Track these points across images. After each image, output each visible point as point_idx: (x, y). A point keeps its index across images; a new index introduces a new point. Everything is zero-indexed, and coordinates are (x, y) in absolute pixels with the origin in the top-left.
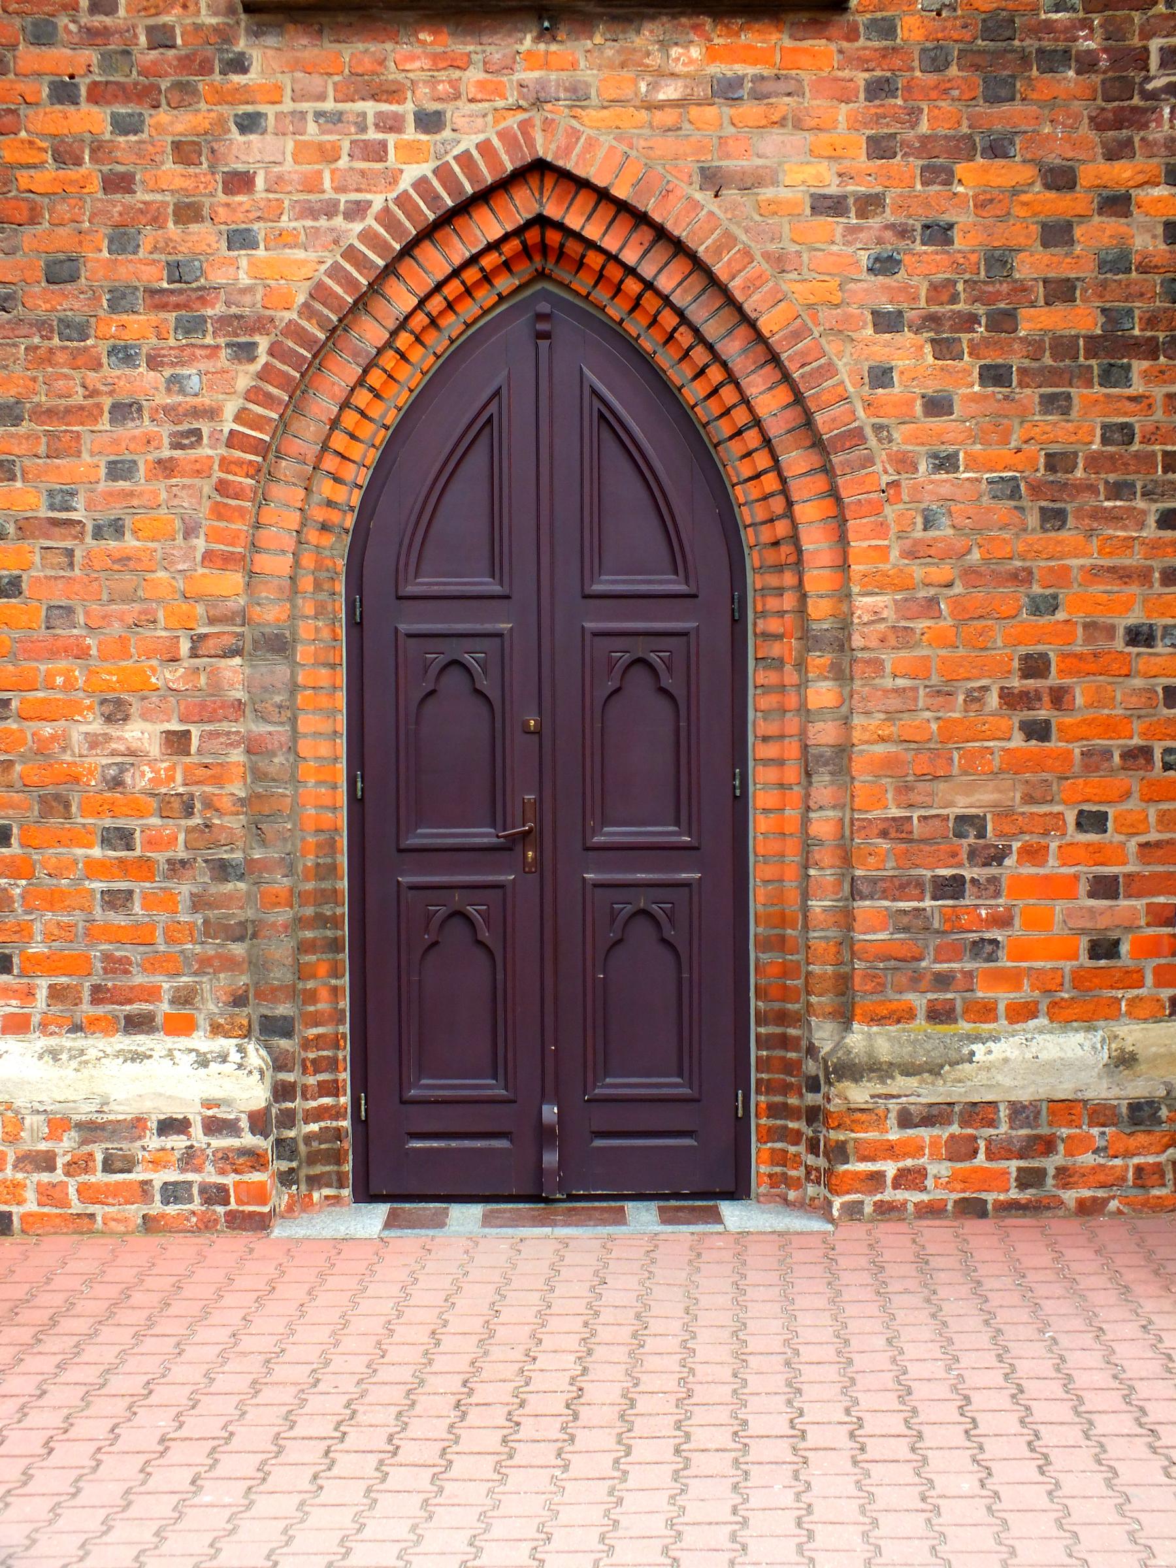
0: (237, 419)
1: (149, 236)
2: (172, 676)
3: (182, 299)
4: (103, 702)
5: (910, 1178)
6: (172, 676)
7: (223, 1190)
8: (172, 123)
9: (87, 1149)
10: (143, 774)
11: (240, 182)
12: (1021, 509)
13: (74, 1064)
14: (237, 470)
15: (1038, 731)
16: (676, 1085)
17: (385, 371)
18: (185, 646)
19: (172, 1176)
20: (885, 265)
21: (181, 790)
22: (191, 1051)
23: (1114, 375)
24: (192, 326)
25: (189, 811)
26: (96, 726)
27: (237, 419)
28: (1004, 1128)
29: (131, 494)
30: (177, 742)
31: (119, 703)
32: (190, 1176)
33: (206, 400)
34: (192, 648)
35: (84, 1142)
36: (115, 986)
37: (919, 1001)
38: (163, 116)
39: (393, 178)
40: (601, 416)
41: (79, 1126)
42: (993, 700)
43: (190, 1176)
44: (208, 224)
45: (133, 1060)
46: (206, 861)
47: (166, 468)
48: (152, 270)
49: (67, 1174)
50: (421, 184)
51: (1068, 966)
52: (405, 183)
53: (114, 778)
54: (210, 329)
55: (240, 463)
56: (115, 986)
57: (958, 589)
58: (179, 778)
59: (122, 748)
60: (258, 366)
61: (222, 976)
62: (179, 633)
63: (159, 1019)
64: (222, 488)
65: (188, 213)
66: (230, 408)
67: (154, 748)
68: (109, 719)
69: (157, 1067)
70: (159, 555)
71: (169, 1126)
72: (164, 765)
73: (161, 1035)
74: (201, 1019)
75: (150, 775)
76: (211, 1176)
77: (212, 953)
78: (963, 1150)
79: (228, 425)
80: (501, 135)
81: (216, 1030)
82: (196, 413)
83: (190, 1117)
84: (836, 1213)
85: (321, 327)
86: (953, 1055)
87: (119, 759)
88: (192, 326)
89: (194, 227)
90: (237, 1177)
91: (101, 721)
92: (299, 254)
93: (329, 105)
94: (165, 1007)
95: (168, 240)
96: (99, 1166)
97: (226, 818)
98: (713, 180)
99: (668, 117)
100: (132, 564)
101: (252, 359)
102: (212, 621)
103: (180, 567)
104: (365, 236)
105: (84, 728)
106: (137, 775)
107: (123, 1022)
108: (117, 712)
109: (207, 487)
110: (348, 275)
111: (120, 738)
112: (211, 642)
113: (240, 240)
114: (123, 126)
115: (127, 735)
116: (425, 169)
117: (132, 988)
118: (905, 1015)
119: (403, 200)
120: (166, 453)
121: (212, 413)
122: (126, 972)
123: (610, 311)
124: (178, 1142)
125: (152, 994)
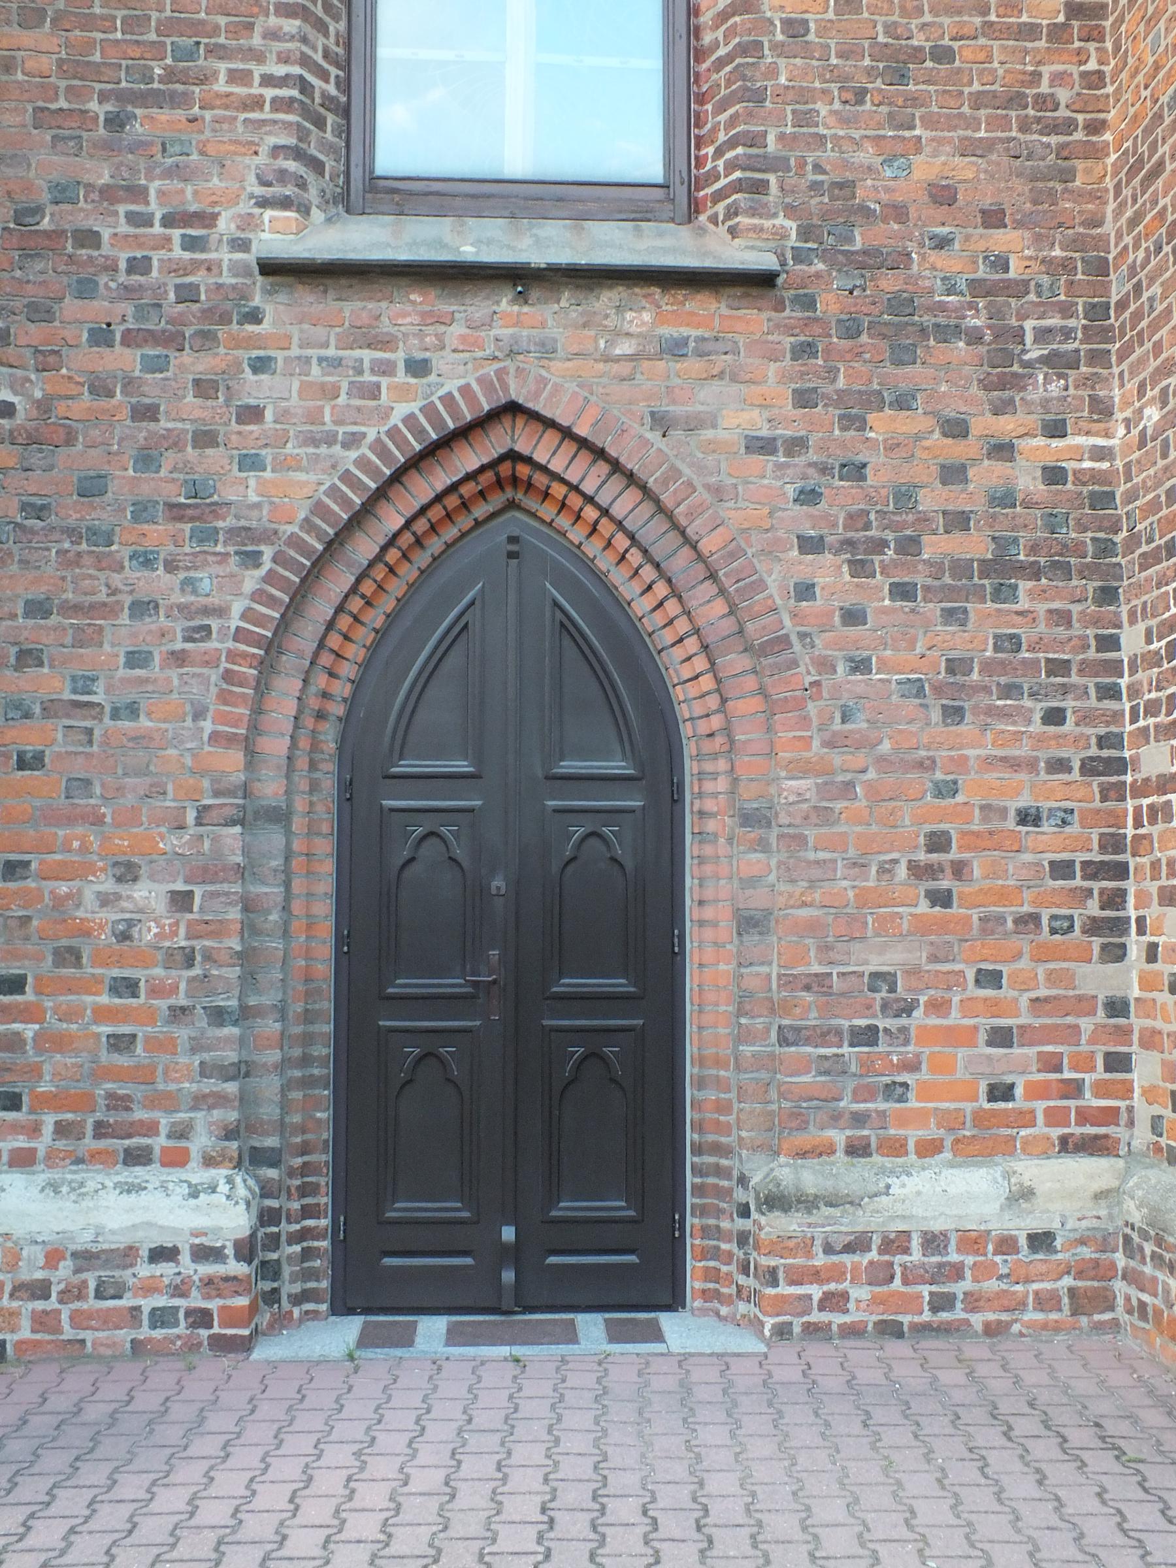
2: (174, 842)
6: (174, 842)
10: (149, 930)
11: (252, 414)
13: (73, 1197)
18: (191, 816)
20: (808, 496)
30: (182, 900)
32: (176, 1302)
33: (215, 600)
37: (839, 1137)
44: (222, 449)
47: (179, 658)
50: (410, 420)
52: (396, 419)
55: (244, 655)
60: (263, 571)
64: (228, 676)
65: (206, 439)
66: (237, 608)
68: (119, 880)
71: (162, 1254)
75: (155, 930)
76: (196, 1301)
80: (480, 380)
82: (206, 611)
85: (319, 540)
91: (112, 881)
93: (331, 352)
98: (662, 423)
99: (625, 368)
108: (128, 873)
109: (214, 676)
116: (414, 407)
119: (393, 433)
122: (128, 1109)
124: (166, 1269)
125: (151, 1129)
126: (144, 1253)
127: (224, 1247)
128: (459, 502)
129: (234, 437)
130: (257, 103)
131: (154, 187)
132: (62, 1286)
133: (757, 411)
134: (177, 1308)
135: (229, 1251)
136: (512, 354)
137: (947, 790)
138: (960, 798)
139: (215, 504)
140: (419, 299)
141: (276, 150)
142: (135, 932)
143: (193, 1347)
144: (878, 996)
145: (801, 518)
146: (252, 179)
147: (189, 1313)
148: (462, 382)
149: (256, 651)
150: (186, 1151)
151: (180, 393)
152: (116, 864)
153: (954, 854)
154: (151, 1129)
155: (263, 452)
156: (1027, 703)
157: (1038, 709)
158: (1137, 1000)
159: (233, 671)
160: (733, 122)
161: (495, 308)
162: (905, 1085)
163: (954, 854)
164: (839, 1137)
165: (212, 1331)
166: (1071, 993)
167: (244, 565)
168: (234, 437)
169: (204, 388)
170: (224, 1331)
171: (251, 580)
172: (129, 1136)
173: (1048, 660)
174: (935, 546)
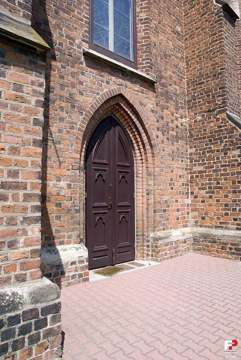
0: (80, 125)
1: (66, 89)
2: (69, 173)
3: (71, 101)
4: (56, 177)
5: (166, 254)
6: (69, 173)
7: (82, 274)
8: (71, 69)
9: (57, 271)
10: (63, 192)
11: (81, 83)
12: (170, 158)
13: (54, 253)
14: (80, 135)
15: (172, 189)
16: (105, 247)
17: (127, 119)
18: (71, 167)
19: (73, 273)
20: (158, 121)
21: (70, 195)
22: (74, 247)
23: (177, 142)
24: (73, 107)
25: (71, 200)
26: (55, 182)
27: (80, 125)
28: (174, 245)
29: (62, 136)
30: (69, 186)
31: (59, 177)
32: (76, 273)
33: (74, 121)
34: (72, 168)
35: (57, 270)
36: (57, 236)
37: (162, 227)
38: (69, 67)
39: (103, 91)
40: (119, 137)
41: (56, 266)
42: (168, 184)
43: (76, 273)
44: (76, 89)
45: (65, 251)
46: (74, 209)
47: (68, 132)
48: (67, 94)
49: (54, 277)
50: (107, 92)
51: (175, 221)
52: (104, 92)
53: (58, 193)
54: (76, 108)
55: (80, 134)
56: (57, 236)
57: (165, 168)
58: (69, 193)
59: (60, 187)
60: (83, 117)
61: (76, 232)
62: (69, 164)
63: (65, 242)
64: (77, 138)
65: (73, 86)
66: (79, 123)
67: (65, 187)
68: (57, 181)
69: (69, 251)
70: (66, 149)
71: (73, 263)
72: (67, 190)
73: (66, 245)
74: (72, 241)
75: (64, 192)
76: (80, 272)
77: (74, 227)
78: (36, 265)
79: (78, 126)
80: (117, 88)
81: (75, 243)
82: (73, 123)
83: (76, 261)
84: (159, 261)
85: (93, 112)
86: (169, 235)
87: (59, 189)
88: (73, 107)
89: (74, 89)
90: (84, 271)
91: (55, 181)
92: (89, 98)
93: (94, 75)
94: (66, 239)
95: (69, 90)
96: (60, 274)
97: (77, 201)
98: (141, 104)
99: (136, 92)
100: (62, 150)
101: (82, 115)
102: (75, 163)
103: (70, 152)
104: (99, 98)
105: (52, 182)
106: (62, 192)
107: (59, 243)
108: (59, 180)
109: (75, 137)
110: (97, 104)
111: (59, 185)
112: (75, 167)
113: (81, 93)
114: (63, 67)
115: (60, 184)
116: (107, 90)
117: (60, 236)
118: (160, 230)
119: (104, 94)
120: (68, 129)
121: (76, 124)
122: (60, 232)
123: (121, 121)
124: (74, 266)
125: (64, 236)
126: (70, 264)
127: (84, 260)
128: (124, 116)
129: (78, 87)
130: (82, 20)
131: (64, 28)
132: (54, 273)
133: (152, 105)
134: (76, 274)
135: (85, 261)
136: (121, 85)
137: (172, 171)
138: (174, 173)
139: (74, 100)
140: (108, 70)
141: (86, 31)
142: (60, 193)
143: (79, 282)
144: (166, 204)
145: (156, 124)
146: (81, 35)
147: (79, 275)
148: (114, 88)
149: (82, 133)
150: (71, 241)
151: (68, 74)
152: (56, 177)
153: (173, 182)
154: (64, 236)
155: (83, 92)
156: (180, 159)
157: (181, 159)
158: (190, 204)
159: (78, 137)
160: (147, 56)
161: (119, 75)
162: (169, 218)
163: (173, 182)
164: (162, 227)
165: (82, 278)
166: (184, 203)
167: (80, 114)
168: (78, 87)
169: (73, 75)
170: (85, 277)
171: (81, 118)
172: (60, 238)
173: (182, 152)
174: (171, 132)
